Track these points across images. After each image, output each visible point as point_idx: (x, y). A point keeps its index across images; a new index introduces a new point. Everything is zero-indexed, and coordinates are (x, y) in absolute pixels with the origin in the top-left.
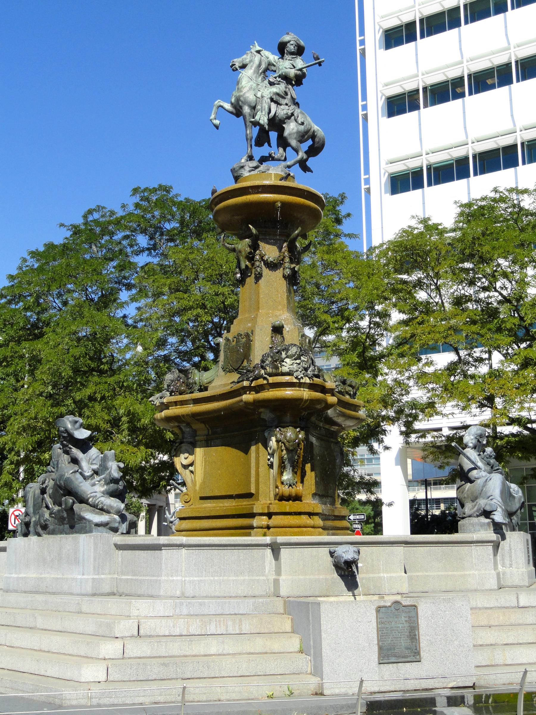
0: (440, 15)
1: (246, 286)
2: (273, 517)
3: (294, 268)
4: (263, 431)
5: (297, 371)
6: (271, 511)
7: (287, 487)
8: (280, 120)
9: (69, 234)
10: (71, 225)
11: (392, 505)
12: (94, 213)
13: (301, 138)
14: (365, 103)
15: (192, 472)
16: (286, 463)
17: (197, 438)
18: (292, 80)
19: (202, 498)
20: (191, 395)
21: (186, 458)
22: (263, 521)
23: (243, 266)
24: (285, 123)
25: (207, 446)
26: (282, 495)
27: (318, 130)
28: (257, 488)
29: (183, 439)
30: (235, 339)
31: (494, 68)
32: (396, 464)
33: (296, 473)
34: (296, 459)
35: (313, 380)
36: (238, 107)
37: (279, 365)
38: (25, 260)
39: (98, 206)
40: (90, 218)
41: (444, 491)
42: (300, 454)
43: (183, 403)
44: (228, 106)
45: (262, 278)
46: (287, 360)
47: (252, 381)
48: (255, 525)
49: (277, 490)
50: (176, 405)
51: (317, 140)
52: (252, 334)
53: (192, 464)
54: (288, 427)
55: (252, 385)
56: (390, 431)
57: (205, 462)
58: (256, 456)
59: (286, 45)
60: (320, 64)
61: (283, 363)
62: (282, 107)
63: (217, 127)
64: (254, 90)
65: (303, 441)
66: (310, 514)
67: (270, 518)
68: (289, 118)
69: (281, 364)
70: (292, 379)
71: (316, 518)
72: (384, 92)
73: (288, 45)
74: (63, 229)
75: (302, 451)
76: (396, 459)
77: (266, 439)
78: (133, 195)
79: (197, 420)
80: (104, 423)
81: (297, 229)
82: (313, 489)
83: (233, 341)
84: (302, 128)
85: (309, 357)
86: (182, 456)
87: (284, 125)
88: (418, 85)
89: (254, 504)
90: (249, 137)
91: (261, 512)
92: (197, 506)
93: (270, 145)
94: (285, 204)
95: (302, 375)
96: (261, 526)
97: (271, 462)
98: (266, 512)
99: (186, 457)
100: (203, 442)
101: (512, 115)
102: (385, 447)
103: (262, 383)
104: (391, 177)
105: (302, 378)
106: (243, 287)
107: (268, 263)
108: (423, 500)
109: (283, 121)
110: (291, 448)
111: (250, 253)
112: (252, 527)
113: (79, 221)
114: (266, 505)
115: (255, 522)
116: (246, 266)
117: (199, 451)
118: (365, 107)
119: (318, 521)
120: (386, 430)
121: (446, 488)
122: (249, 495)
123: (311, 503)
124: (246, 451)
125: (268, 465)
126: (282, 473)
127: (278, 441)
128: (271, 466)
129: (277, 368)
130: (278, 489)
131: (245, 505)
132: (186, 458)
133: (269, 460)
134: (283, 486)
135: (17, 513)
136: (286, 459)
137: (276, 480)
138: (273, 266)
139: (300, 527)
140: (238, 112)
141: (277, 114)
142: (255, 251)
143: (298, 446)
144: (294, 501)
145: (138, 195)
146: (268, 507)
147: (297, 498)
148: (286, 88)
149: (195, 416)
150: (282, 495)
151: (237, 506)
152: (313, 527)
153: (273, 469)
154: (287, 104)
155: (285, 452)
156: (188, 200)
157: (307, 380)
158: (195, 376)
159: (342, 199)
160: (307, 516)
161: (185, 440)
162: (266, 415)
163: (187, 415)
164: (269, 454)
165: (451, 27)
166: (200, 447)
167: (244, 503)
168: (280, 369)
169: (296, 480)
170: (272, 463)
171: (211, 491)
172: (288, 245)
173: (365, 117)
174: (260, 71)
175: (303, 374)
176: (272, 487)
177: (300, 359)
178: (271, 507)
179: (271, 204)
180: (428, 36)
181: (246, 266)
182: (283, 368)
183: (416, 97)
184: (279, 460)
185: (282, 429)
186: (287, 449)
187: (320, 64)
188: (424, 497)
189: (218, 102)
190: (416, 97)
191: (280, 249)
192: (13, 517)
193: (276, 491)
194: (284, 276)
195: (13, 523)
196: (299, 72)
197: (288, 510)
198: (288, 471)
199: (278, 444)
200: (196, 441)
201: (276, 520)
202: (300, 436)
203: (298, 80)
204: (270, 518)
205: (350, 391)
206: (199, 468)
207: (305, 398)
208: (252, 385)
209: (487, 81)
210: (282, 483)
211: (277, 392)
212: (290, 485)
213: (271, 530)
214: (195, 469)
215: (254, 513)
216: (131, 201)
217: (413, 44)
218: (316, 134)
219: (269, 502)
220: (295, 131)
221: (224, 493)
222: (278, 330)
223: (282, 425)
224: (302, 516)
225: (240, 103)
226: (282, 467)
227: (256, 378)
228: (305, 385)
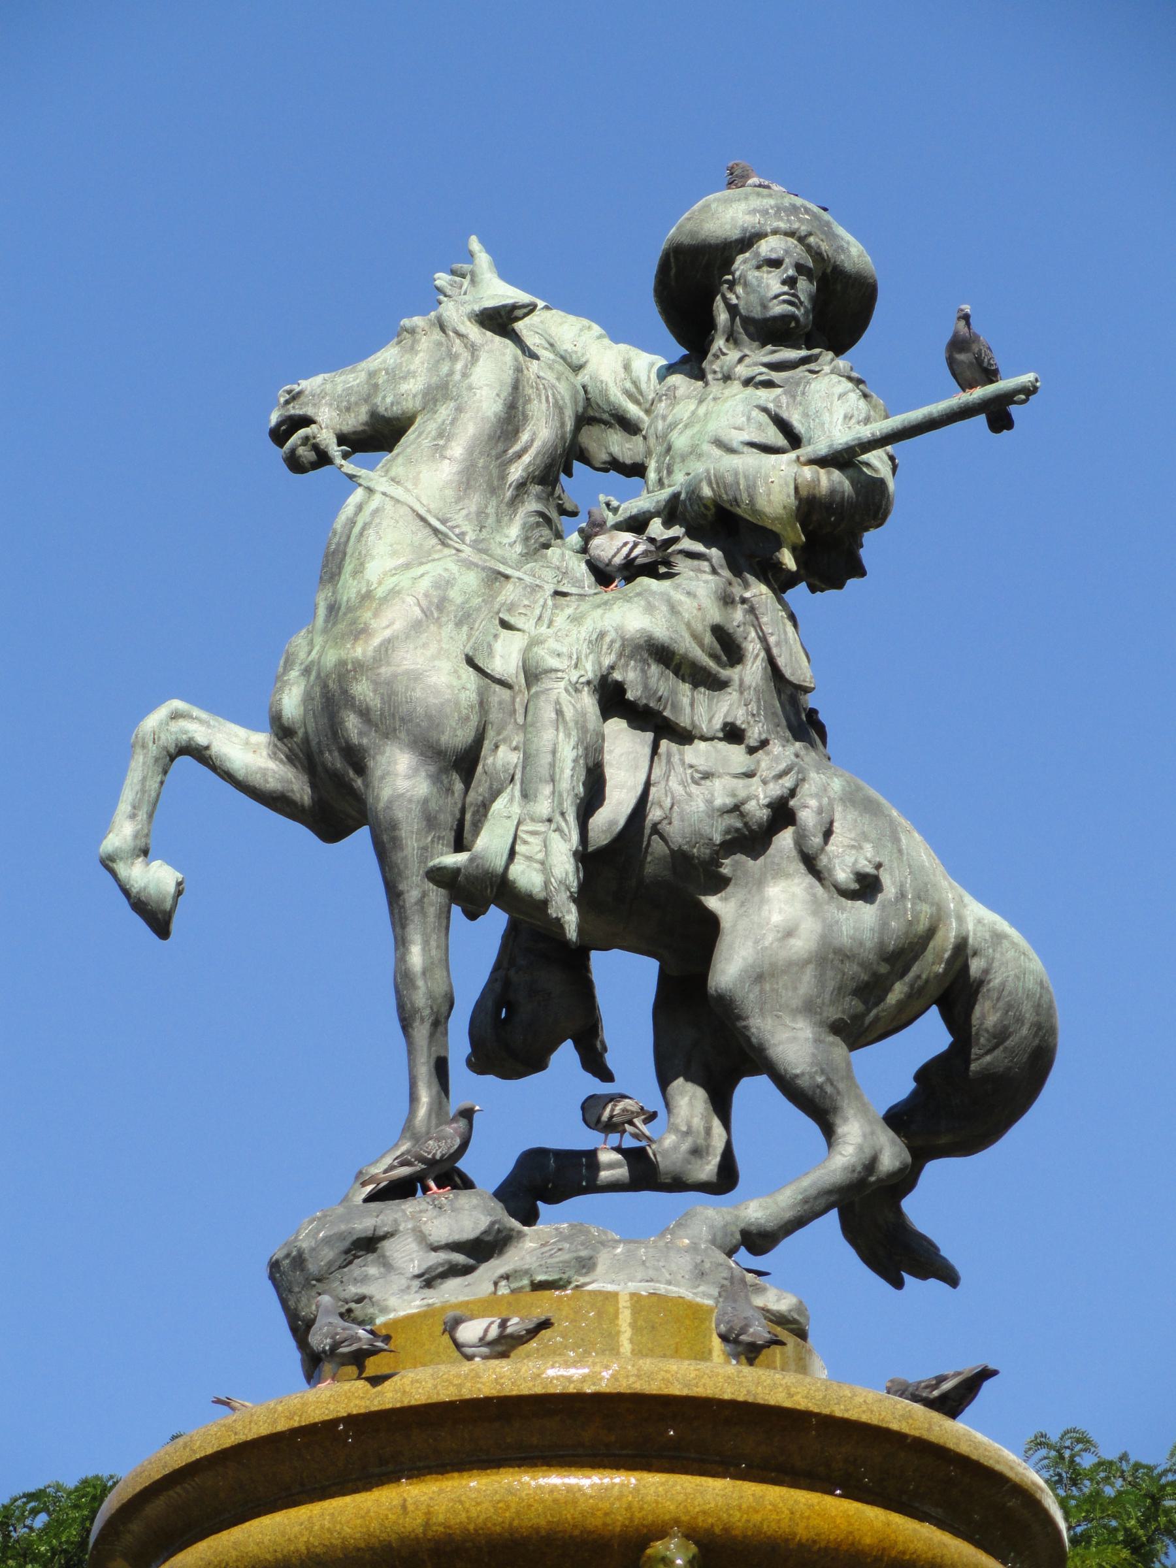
8: (681, 859)
13: (854, 1005)
24: (719, 884)
27: (998, 937)
36: (333, 759)
44: (247, 750)
59: (727, 265)
60: (998, 415)
62: (698, 754)
63: (158, 920)
64: (465, 619)
68: (752, 839)
73: (742, 264)
84: (860, 921)
87: (712, 902)
109: (699, 871)
141: (654, 814)
148: (727, 601)
154: (733, 734)
174: (516, 472)
187: (998, 415)
196: (829, 480)
220: (803, 944)
225: (352, 723)
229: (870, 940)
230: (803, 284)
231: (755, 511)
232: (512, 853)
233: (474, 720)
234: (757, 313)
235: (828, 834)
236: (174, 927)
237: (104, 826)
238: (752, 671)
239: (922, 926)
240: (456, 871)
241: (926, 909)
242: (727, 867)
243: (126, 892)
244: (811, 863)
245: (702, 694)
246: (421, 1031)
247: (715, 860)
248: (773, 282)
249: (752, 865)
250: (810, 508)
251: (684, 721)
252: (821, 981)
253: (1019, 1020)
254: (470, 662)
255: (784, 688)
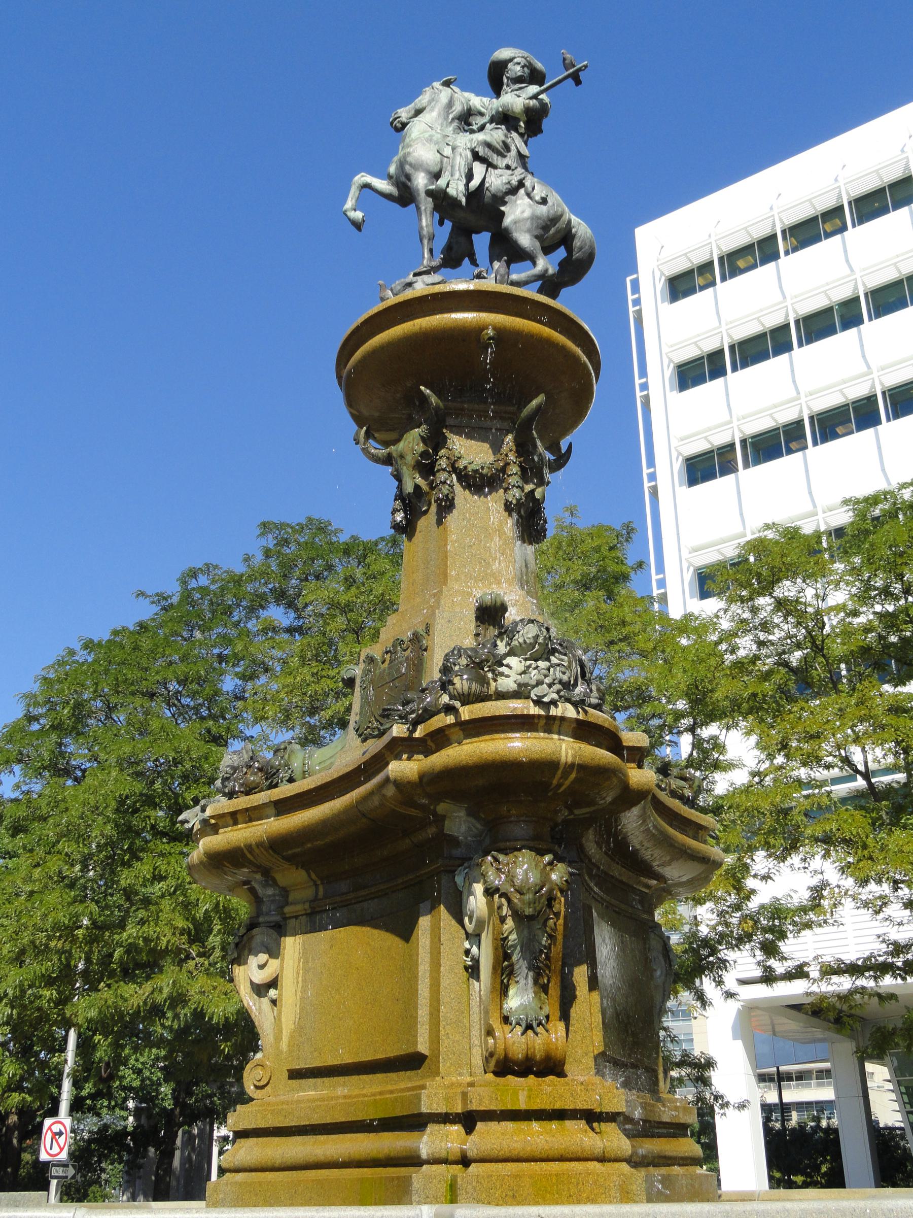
0: (760, 337)
1: (418, 536)
2: (479, 1125)
3: (533, 491)
4: (452, 872)
5: (539, 683)
6: (474, 1106)
7: (519, 1030)
8: (494, 196)
9: (156, 609)
10: (157, 595)
11: (745, 1106)
12: (200, 575)
13: (541, 232)
14: (652, 470)
15: (274, 1002)
16: (515, 958)
17: (288, 910)
18: (517, 120)
19: (296, 1074)
20: (269, 792)
21: (261, 967)
22: (449, 1139)
23: (409, 488)
24: (505, 203)
25: (313, 930)
26: (506, 1056)
27: (579, 224)
28: (435, 1038)
29: (258, 916)
30: (387, 657)
31: (848, 405)
32: (735, 1038)
33: (545, 989)
34: (546, 951)
35: (586, 712)
36: (403, 179)
37: (490, 675)
38: (72, 653)
39: (207, 565)
40: (193, 584)
41: (796, 1091)
42: (554, 930)
43: (252, 815)
44: (382, 185)
45: (455, 511)
46: (512, 661)
47: (415, 724)
48: (424, 1153)
49: (491, 1041)
50: (236, 823)
51: (577, 243)
52: (428, 632)
53: (273, 983)
54: (519, 850)
55: (417, 734)
56: (735, 962)
57: (306, 970)
58: (432, 942)
59: (506, 67)
60: (576, 78)
61: (503, 669)
62: (498, 171)
63: (358, 225)
64: (437, 143)
65: (562, 891)
66: (591, 1117)
67: (469, 1129)
68: (513, 191)
69: (493, 671)
70: (528, 708)
71: (611, 1130)
72: (681, 449)
73: (510, 65)
74: (144, 602)
75: (561, 921)
76: (734, 1028)
77: (461, 893)
78: (262, 534)
79: (288, 859)
80: (174, 934)
81: (536, 396)
82: (597, 1041)
83: (383, 662)
84: (543, 210)
85: (574, 656)
86: (254, 961)
87: (502, 208)
88: (733, 436)
89: (423, 1087)
90: (425, 232)
91: (442, 1109)
92: (282, 1097)
93: (474, 263)
94: (503, 336)
95: (555, 696)
96: (443, 1154)
97: (473, 959)
98: (459, 1109)
99: (262, 962)
100: (304, 919)
101: (883, 470)
102: (726, 992)
103: (441, 725)
104: (699, 574)
105: (554, 703)
106: (410, 539)
107: (467, 475)
108: (775, 1105)
109: (500, 199)
110: (528, 911)
111: (424, 455)
112: (414, 1161)
113: (174, 589)
114: (459, 1090)
115: (428, 1142)
116: (417, 487)
117: (291, 945)
118: (652, 477)
119: (613, 1139)
120: (726, 961)
121: (798, 1085)
122: (413, 1062)
123: (588, 1082)
124: (406, 932)
125: (466, 968)
126: (504, 991)
127: (489, 892)
128: (473, 970)
129: (484, 681)
130: (494, 1037)
131: (402, 1090)
132: (261, 967)
133: (467, 952)
134: (508, 1028)
135: (56, 1128)
136: (514, 946)
137: (487, 1012)
138: (479, 482)
139: (562, 1159)
140: (405, 195)
141: (487, 185)
142: (436, 450)
143: (550, 906)
144: (541, 1074)
145: (270, 536)
146: (464, 1095)
147: (550, 1066)
148: (506, 136)
149: (278, 845)
150: (506, 1056)
151: (381, 1093)
152: (602, 1159)
153: (478, 979)
154: (508, 167)
155: (510, 923)
156: (354, 538)
157: (570, 712)
158: (293, 757)
159: (628, 533)
160: (582, 1124)
161: (261, 919)
162: (459, 823)
163: (260, 844)
164: (468, 936)
165: (777, 353)
166: (294, 934)
167: (402, 1085)
168: (493, 684)
169: (547, 1009)
170: (476, 961)
171: (316, 1054)
172: (516, 440)
173: (654, 492)
174: (451, 116)
175: (558, 692)
176: (476, 1032)
177: (548, 660)
178: (470, 1095)
179: (471, 335)
180: (742, 368)
181: (417, 487)
182: (501, 680)
183: (730, 457)
184: (496, 949)
185: (501, 857)
186: (517, 915)
187: (576, 78)
188: (776, 1100)
189: (364, 178)
190: (730, 457)
191: (496, 447)
192: (49, 1135)
193: (486, 1042)
194: (508, 508)
195: (48, 1147)
196: (533, 103)
197: (522, 1105)
198: (522, 982)
199: (490, 904)
200: (285, 919)
201: (490, 1137)
202: (554, 877)
203: (532, 122)
204: (469, 1129)
205: (682, 788)
206: (289, 992)
207: (563, 759)
208: (417, 734)
209: (837, 430)
210: (506, 1020)
211: (483, 745)
212: (529, 1027)
213: (473, 1167)
214: (280, 995)
215: (420, 1115)
216: (256, 546)
217: (720, 381)
218: (574, 230)
219: (469, 1079)
220: (527, 214)
221: (348, 1059)
222: (490, 614)
223: (502, 845)
224: (568, 1123)
225: (407, 168)
226: (503, 970)
227: (428, 714)
228: (565, 724)
229: (545, 215)
230: (526, 69)
231: (513, 112)
232: (448, 184)
233: (439, 166)
234: (514, 76)
235: (533, 189)
236: (363, 229)
237: (345, 202)
238: (513, 152)
239: (559, 213)
240: (432, 190)
241: (560, 209)
242: (507, 199)
243: (350, 220)
244: (528, 195)
245: (499, 158)
246: (425, 242)
247: (503, 197)
248: (518, 68)
249: (513, 198)
250: (528, 110)
251: (495, 163)
252: (532, 224)
253: (586, 244)
254: (438, 151)
255: (521, 156)
